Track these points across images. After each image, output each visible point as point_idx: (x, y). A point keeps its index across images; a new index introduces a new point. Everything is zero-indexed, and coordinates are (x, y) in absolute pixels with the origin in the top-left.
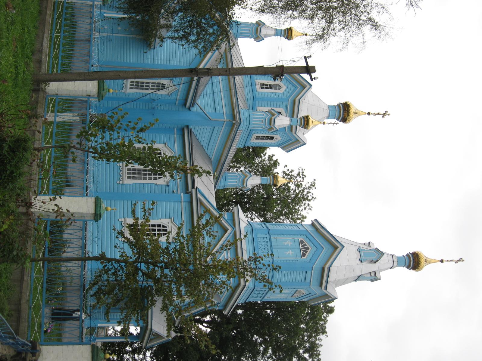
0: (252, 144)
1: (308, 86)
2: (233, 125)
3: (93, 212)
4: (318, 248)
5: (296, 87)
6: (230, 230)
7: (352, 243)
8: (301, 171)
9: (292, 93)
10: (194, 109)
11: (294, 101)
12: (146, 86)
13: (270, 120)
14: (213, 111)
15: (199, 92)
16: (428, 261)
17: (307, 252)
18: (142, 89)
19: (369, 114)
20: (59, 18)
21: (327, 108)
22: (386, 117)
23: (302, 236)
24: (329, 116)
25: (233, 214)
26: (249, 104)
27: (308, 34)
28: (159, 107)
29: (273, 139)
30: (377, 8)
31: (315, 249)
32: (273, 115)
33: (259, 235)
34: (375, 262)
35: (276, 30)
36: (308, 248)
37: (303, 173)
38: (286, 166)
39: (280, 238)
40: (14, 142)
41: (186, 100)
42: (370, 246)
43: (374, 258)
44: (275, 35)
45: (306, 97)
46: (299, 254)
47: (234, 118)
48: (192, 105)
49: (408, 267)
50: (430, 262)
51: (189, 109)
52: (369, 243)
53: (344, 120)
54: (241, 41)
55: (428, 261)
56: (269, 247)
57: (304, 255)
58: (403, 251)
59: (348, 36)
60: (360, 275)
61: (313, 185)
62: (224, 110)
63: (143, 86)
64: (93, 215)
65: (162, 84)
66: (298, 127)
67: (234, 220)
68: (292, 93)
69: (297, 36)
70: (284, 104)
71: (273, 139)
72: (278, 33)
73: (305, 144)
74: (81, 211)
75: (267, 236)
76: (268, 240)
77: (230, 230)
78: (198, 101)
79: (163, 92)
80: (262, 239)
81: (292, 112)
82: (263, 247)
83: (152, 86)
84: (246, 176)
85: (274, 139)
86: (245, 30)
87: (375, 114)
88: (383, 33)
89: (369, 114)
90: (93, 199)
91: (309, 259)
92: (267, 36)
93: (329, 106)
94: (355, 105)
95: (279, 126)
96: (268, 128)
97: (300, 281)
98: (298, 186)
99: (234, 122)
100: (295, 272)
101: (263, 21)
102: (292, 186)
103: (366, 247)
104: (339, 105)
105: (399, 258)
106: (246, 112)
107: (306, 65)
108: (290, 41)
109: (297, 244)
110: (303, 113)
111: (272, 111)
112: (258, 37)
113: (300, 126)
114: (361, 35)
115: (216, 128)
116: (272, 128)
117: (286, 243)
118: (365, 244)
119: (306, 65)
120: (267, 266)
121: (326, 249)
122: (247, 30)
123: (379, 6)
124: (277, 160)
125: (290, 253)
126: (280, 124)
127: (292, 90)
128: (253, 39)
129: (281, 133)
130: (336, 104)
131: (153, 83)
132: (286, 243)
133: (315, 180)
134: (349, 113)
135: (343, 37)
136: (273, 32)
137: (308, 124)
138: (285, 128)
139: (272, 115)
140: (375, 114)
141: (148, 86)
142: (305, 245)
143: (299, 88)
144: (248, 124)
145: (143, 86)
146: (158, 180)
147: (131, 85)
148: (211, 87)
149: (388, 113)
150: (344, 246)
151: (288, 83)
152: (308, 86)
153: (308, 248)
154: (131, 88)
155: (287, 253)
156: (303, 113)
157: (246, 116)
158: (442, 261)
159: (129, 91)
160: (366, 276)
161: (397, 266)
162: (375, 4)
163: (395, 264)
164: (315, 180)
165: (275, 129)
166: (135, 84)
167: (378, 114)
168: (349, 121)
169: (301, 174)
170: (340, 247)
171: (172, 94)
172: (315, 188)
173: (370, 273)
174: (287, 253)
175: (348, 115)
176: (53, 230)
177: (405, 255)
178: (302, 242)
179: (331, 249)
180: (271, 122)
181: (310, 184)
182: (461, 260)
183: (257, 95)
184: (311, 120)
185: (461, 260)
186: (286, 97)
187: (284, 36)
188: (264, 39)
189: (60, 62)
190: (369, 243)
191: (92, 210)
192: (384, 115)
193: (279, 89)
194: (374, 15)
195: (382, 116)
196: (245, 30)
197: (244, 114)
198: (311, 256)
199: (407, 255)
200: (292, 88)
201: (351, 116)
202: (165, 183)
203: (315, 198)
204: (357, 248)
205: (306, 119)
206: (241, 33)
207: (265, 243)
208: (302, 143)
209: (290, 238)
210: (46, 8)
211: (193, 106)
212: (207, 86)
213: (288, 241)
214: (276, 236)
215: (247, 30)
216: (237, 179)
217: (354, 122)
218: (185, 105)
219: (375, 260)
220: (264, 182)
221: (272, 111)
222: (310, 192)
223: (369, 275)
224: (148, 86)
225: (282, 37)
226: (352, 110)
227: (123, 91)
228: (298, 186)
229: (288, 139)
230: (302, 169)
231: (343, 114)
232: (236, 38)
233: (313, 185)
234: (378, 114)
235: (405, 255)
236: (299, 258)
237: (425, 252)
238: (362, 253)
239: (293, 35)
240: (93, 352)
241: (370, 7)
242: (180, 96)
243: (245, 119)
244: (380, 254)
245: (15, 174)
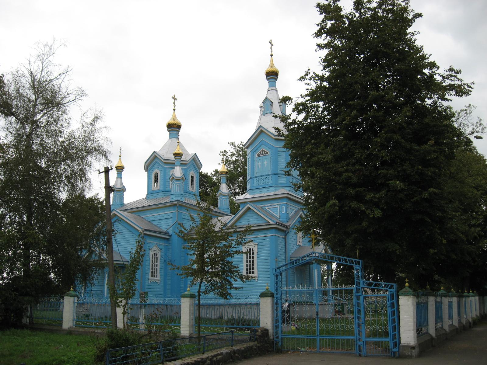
0: (197, 191)
1: (155, 154)
2: (180, 206)
3: (189, 298)
4: (262, 143)
5: (156, 162)
6: (248, 206)
7: (260, 120)
8: (222, 154)
9: (160, 165)
10: (171, 233)
11: (165, 163)
12: (155, 266)
13: (177, 180)
14: (171, 220)
15: (159, 230)
16: (272, 65)
17: (265, 151)
18: (157, 269)
19: (174, 110)
20: (84, 324)
21: (171, 139)
22: (176, 97)
23: (255, 155)
24: (176, 138)
25: (241, 203)
26: (167, 195)
27: (120, 155)
28: (170, 257)
29: (193, 177)
30: (84, 119)
31: (263, 145)
32: (173, 178)
33: (255, 185)
34: (272, 103)
35: (117, 177)
36: (263, 151)
37: (223, 152)
38: (219, 164)
39: (256, 171)
40: (228, 362)
41: (164, 238)
42: (262, 107)
43: (269, 104)
44: (121, 178)
45: (163, 154)
46: (267, 157)
47: (175, 205)
48: (168, 234)
49: (276, 80)
50: (273, 64)
51: (170, 236)
52: (260, 107)
53: (179, 127)
54: (126, 201)
55: (272, 65)
56: (262, 177)
57: (267, 153)
58: (265, 83)
59: (101, 137)
60: (281, 113)
61: (232, 144)
62: (170, 212)
63: (154, 269)
64: (192, 298)
65: (153, 255)
66: (182, 159)
67: (245, 202)
68: (160, 165)
69: (122, 163)
70: (167, 170)
71: (193, 177)
72: (119, 176)
73: (195, 154)
74: (189, 306)
75: (255, 179)
76: (258, 178)
77: (248, 206)
78: (165, 230)
79: (159, 255)
80: (257, 183)
81: (170, 164)
82: (262, 182)
83: (155, 262)
84: (221, 193)
85: (192, 175)
86: (118, 199)
87: (175, 106)
88: (99, 115)
89: (174, 110)
90: (182, 299)
91: (270, 150)
92: (122, 184)
93: (170, 138)
94: (168, 119)
95: (181, 173)
96: (182, 181)
97: (284, 155)
98: (233, 155)
99: (178, 205)
100: (279, 159)
101: (266, 128)
102: (234, 158)
103: (262, 109)
104: (169, 131)
105: (270, 86)
106: (172, 197)
107: (104, 173)
108: (125, 167)
109: (260, 158)
110: (172, 157)
111: (170, 179)
112: (122, 190)
113: (181, 159)
114: (101, 129)
115: (183, 217)
116: (183, 178)
117: (260, 166)
118: (261, 110)
119: (104, 173)
120: (478, 125)
121: (262, 138)
122: (118, 198)
123: (83, 118)
124: (214, 171)
125: (266, 163)
126: (179, 173)
127: (158, 165)
128: (124, 193)
129: (188, 171)
130: (168, 133)
131: (152, 262)
132: (260, 166)
133: (229, 143)
134: (173, 124)
135: (103, 141)
136: (119, 179)
137: (179, 154)
138: (182, 169)
139: (173, 178)
140: (175, 106)
141: (155, 265)
142: (260, 152)
143: (156, 160)
144: (180, 195)
145: (154, 269)
146: (254, 251)
147: (154, 277)
148: (156, 222)
149: (174, 96)
150: (260, 126)
151: (154, 167)
152: (155, 154)
153: (263, 151)
154: (157, 277)
155: (266, 165)
156: (172, 157)
157: (174, 196)
158: (272, 55)
159: (158, 278)
160: (282, 109)
161: (275, 87)
162: (82, 121)
163: (274, 88)
164: (229, 143)
165: (183, 176)
166: (153, 274)
167: (174, 103)
168: (179, 123)
169: (224, 153)
170: (261, 128)
171: (160, 249)
172: (234, 142)
173: (280, 106)
174: (266, 165)
175: (175, 124)
176: (202, 321)
177: (268, 82)
178: (258, 155)
179: (263, 134)
180: (178, 179)
181: (232, 146)
182: (271, 42)
183: (162, 189)
184: (176, 152)
185: (271, 42)
186: (162, 169)
187: (122, 172)
188: (124, 186)
189: (109, 322)
190: (260, 107)
191: (188, 299)
192: (174, 98)
193: (157, 174)
194: (89, 120)
195: (176, 100)
196: (118, 199)
197: (173, 198)
198: (268, 148)
199: (268, 80)
200: (157, 165)
201: (175, 122)
202: (256, 246)
203: (241, 142)
204: (263, 116)
205: (176, 155)
206: (120, 202)
207: (265, 179)
208: (195, 156)
209: (256, 163)
210: (78, 331)
211: (168, 233)
212: (155, 224)
213: (258, 164)
214: (255, 173)
215: (118, 198)
216: (223, 200)
217: (180, 120)
218: (168, 239)
219: (271, 103)
220: (225, 181)
221: (170, 179)
222: (238, 146)
223: (282, 106)
224: (155, 265)
225: (122, 173)
226: (172, 122)
227: (159, 282)
228: (233, 155)
229: (192, 166)
230: (221, 153)
231: (175, 128)
232: (124, 205)
233: (232, 144)
234: (174, 103)
235: (268, 82)
236: (269, 156)
237: (266, 67)
238: (266, 112)
239: (120, 165)
240: (263, 297)
241: (83, 124)
242: (162, 243)
243: (176, 197)
244: (267, 100)
245: (125, 338)
